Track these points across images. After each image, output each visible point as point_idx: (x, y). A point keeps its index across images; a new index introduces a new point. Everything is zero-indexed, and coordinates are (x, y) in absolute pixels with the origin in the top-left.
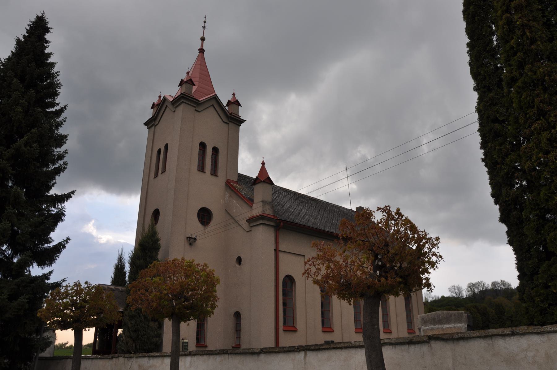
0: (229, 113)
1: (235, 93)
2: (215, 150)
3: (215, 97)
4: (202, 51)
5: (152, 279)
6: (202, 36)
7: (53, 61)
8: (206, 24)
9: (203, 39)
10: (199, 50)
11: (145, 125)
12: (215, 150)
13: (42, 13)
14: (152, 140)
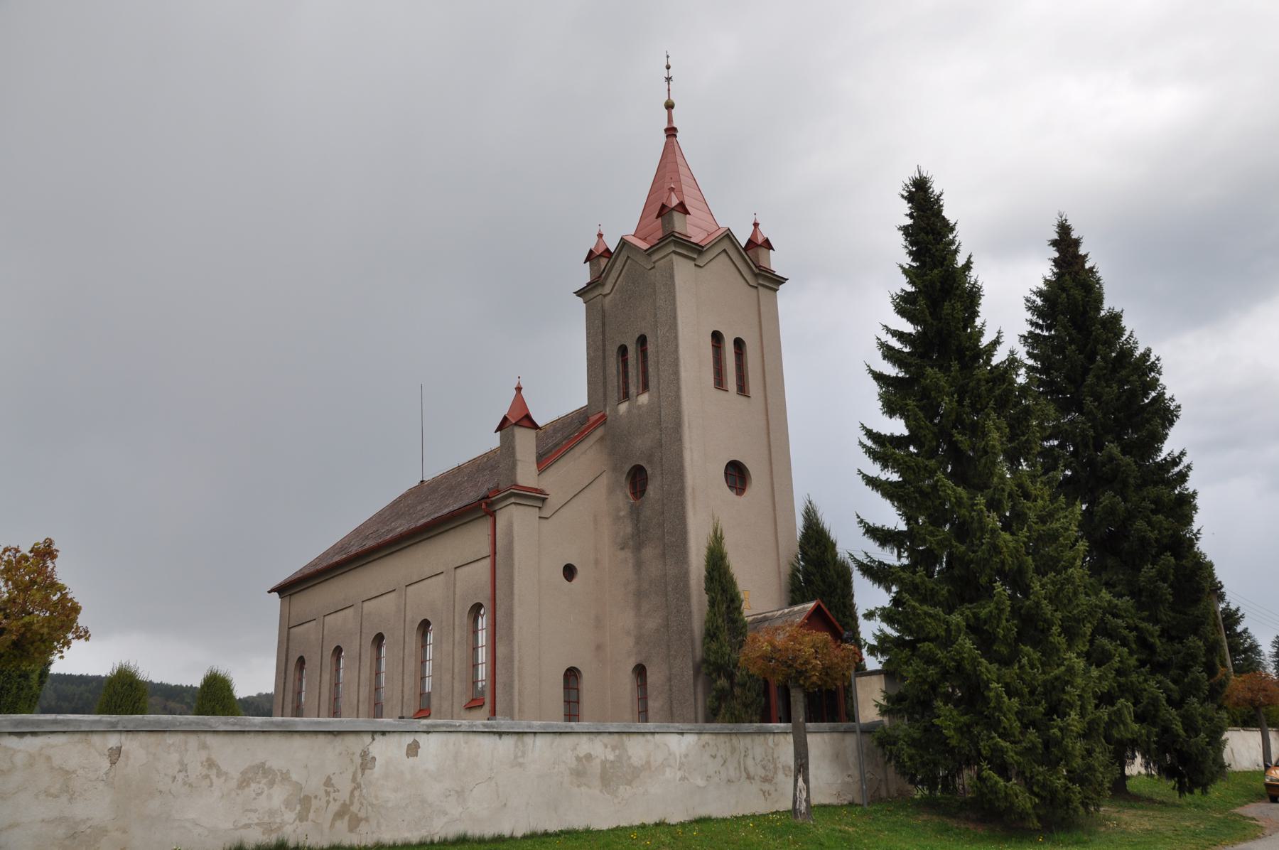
0: (608, 262)
1: (759, 222)
2: (739, 344)
3: (728, 235)
4: (671, 132)
5: (1115, 497)
6: (667, 99)
7: (908, 218)
8: (665, 73)
9: (669, 106)
10: (666, 130)
12: (739, 344)
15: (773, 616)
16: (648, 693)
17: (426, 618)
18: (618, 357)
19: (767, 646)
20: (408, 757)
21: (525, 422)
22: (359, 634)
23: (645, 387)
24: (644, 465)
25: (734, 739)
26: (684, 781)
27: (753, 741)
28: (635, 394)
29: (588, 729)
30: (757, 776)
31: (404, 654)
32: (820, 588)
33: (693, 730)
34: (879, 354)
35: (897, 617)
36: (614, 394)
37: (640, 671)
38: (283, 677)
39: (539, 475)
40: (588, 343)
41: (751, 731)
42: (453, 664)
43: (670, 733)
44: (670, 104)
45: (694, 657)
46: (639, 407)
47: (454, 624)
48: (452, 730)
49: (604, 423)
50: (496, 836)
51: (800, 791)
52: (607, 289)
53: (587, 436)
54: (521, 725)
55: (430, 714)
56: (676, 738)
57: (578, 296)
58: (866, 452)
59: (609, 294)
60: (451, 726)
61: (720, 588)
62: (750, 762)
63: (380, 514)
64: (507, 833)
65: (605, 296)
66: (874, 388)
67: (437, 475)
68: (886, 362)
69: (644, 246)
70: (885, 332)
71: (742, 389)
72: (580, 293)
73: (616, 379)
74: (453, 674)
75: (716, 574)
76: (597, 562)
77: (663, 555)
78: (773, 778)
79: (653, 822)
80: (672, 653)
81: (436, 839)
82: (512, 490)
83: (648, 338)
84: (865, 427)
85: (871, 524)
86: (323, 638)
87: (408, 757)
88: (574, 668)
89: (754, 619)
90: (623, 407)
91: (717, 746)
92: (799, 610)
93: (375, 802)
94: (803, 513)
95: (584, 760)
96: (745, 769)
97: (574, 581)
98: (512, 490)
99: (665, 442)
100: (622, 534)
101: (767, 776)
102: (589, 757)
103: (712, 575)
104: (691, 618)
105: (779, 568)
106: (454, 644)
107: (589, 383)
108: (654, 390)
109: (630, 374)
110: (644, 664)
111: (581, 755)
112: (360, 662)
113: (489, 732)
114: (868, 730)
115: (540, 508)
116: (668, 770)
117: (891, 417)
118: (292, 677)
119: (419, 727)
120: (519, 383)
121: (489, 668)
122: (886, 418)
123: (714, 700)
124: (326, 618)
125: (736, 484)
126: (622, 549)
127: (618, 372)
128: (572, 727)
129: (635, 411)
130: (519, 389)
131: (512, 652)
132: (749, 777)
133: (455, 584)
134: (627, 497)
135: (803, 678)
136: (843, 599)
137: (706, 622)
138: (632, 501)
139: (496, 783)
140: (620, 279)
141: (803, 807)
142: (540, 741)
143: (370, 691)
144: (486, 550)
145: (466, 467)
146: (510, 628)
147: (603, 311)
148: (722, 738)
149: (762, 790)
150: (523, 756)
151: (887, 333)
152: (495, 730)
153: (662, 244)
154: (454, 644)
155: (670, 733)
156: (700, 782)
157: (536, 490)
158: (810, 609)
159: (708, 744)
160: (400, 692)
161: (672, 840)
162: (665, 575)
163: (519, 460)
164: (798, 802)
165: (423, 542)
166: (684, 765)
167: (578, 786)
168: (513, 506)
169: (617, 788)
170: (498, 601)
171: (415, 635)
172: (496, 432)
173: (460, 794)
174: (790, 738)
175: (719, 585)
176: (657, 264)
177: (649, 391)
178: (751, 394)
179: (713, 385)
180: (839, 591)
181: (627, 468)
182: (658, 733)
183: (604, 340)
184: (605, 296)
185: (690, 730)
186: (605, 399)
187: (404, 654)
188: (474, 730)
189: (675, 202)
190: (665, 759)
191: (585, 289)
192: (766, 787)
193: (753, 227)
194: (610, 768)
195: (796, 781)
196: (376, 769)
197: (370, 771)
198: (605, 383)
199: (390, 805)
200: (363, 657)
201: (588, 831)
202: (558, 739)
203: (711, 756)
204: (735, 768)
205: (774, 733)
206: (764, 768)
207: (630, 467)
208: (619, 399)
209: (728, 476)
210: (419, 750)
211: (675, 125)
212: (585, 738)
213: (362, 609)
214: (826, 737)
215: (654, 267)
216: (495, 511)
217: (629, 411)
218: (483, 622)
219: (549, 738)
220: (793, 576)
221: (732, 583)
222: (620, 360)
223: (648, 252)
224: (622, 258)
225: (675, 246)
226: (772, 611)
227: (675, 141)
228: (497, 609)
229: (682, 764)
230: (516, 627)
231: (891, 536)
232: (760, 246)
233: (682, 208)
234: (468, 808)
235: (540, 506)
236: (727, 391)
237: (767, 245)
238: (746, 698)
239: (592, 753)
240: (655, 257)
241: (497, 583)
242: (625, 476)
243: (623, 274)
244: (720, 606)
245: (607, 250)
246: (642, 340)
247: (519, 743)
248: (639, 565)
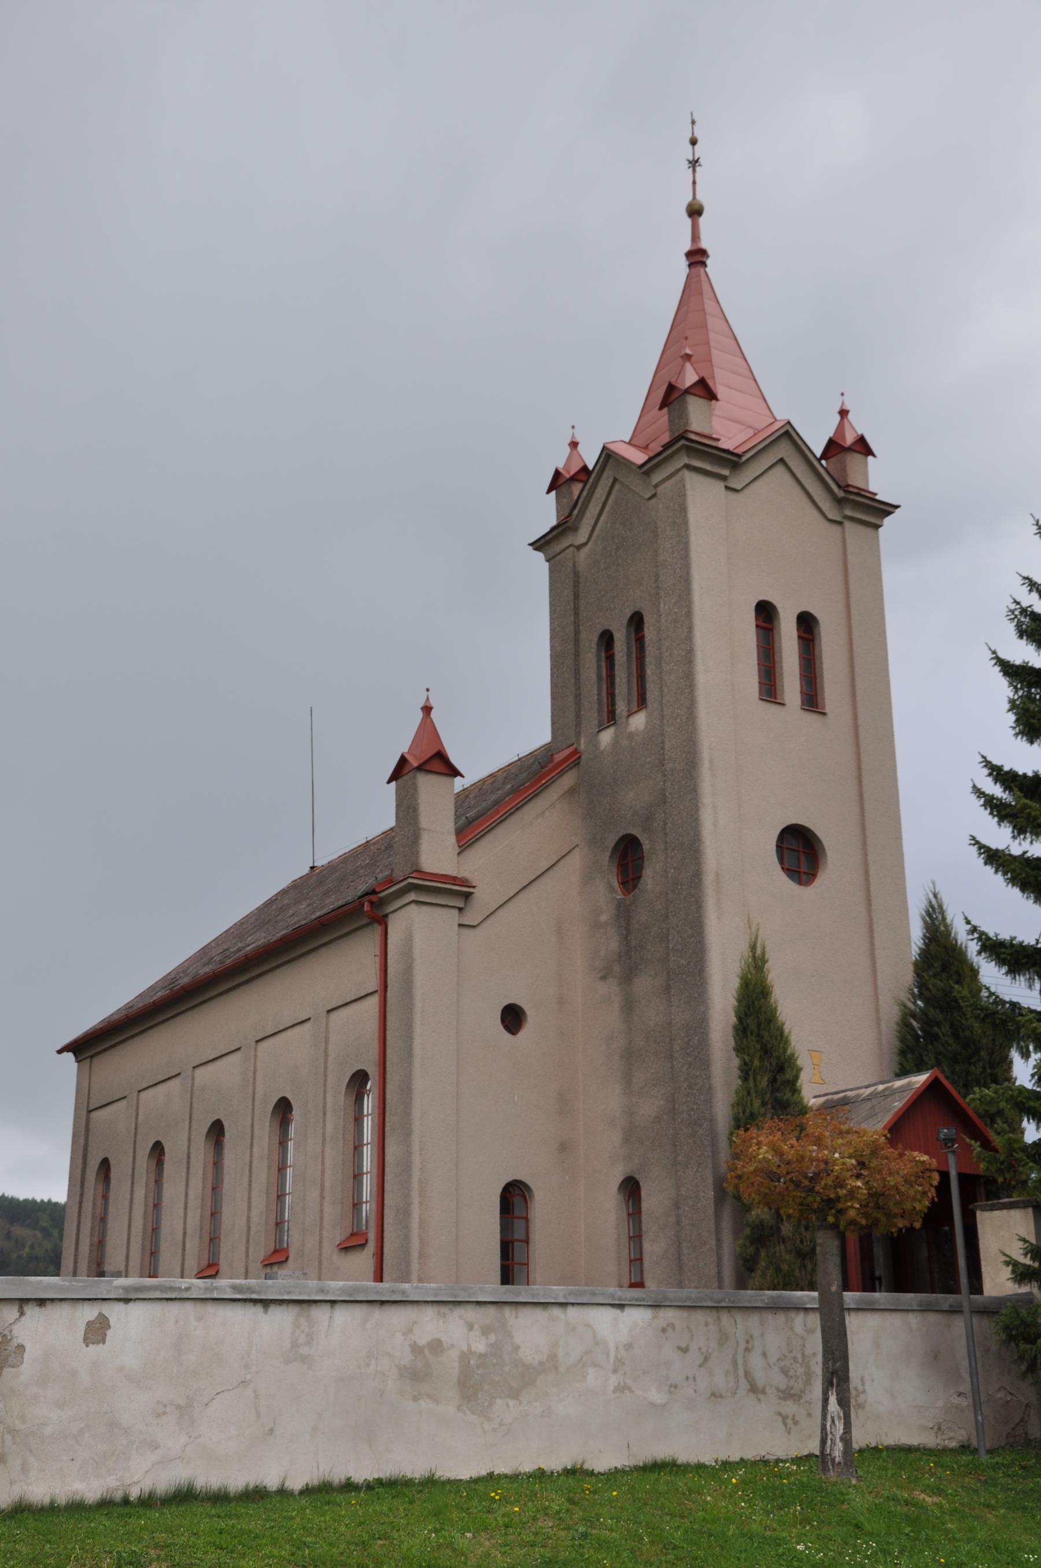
2: (807, 623)
3: (787, 433)
4: (697, 257)
9: (695, 212)
10: (689, 254)
11: (537, 549)
12: (807, 623)
13: (1035, 523)
14: (857, 670)
15: (859, 1096)
16: (644, 1229)
17: (285, 1095)
18: (599, 650)
19: (767, 1152)
20: (87, 1346)
21: (437, 765)
22: (187, 1122)
23: (642, 702)
24: (638, 836)
25: (726, 1319)
26: (623, 1392)
27: (762, 1322)
28: (625, 714)
29: (435, 1296)
30: (771, 1386)
31: (251, 1156)
32: (949, 1048)
33: (643, 1300)
34: (1011, 628)
35: (1032, 1104)
36: (591, 715)
37: (631, 1188)
38: (79, 1193)
39: (459, 854)
40: (552, 630)
41: (760, 1304)
42: (323, 1172)
43: (598, 1304)
44: (696, 207)
45: (715, 1167)
46: (631, 736)
47: (325, 1106)
48: (173, 1296)
49: (577, 764)
50: (251, 1486)
51: (833, 1421)
52: (581, 536)
53: (546, 787)
54: (309, 1289)
55: (287, 1259)
56: (609, 1313)
57: (536, 549)
58: (985, 805)
59: (585, 544)
60: (172, 1289)
61: (758, 1046)
62: (756, 1362)
63: (242, 923)
64: (272, 1483)
65: (579, 548)
66: (1003, 690)
67: (336, 856)
68: (1024, 642)
69: (638, 457)
70: (1026, 589)
71: (812, 700)
72: (540, 545)
73: (595, 687)
74: (322, 1189)
75: (752, 1023)
76: (561, 1001)
77: (667, 989)
78: (803, 1391)
79: (559, 1468)
80: (680, 1158)
81: (134, 1494)
82: (410, 880)
83: (645, 617)
84: (990, 762)
85: (992, 935)
86: (136, 1128)
87: (87, 1346)
88: (515, 1181)
89: (827, 1100)
90: (606, 737)
91: (691, 1331)
92: (902, 1086)
93: (19, 1426)
94: (923, 913)
95: (427, 1352)
96: (747, 1374)
97: (522, 1034)
98: (410, 880)
99: (670, 794)
100: (602, 953)
101: (792, 1388)
102: (436, 1346)
103: (745, 1024)
104: (710, 1099)
105: (877, 1010)
106: (324, 1140)
107: (553, 698)
108: (655, 706)
109: (617, 680)
110: (637, 1176)
111: (422, 1342)
112: (188, 1168)
113: (245, 1300)
114: (990, 1310)
115: (460, 909)
116: (592, 1373)
117: (1032, 743)
118: (92, 1192)
119: (109, 1291)
120: (428, 699)
121: (375, 1180)
122: (1022, 743)
123: (747, 1244)
124: (143, 1095)
125: (799, 866)
126: (604, 978)
127: (599, 677)
128: (403, 1292)
129: (625, 743)
130: (427, 709)
131: (409, 1153)
132: (754, 1389)
133: (327, 1038)
134: (612, 889)
135: (834, 1211)
136: (991, 1067)
137: (733, 1106)
138: (620, 896)
139: (255, 1391)
140: (602, 518)
141: (837, 1452)
142: (342, 1316)
143: (202, 1217)
144: (372, 983)
145: (375, 844)
146: (407, 1113)
147: (576, 574)
148: (700, 1317)
149: (780, 1414)
150: (308, 1344)
151: (1031, 591)
152: (254, 1296)
153: (670, 451)
154: (324, 1140)
155: (598, 1304)
156: (656, 1396)
157: (454, 880)
158: (918, 1086)
159: (672, 1326)
160: (245, 1219)
161: (567, 1505)
162: (670, 1024)
163: (425, 830)
164: (829, 1442)
165: (282, 969)
166: (623, 1364)
167: (415, 1399)
168: (413, 906)
169: (490, 1405)
170: (389, 1068)
171: (268, 1124)
172: (389, 782)
173: (185, 1411)
174: (814, 1320)
175: (758, 1042)
176: (659, 489)
177: (646, 707)
178: (827, 710)
179: (757, 695)
180: (983, 1053)
181: (612, 840)
182: (573, 1304)
183: (576, 624)
184: (579, 548)
185: (637, 1300)
186: (578, 725)
187: (251, 1156)
188: (215, 1296)
189: (690, 377)
190: (586, 1353)
191: (547, 538)
192: (790, 1408)
193: (838, 418)
194: (478, 1367)
195: (826, 1401)
196: (25, 1367)
197: (13, 1370)
198: (578, 697)
199: (48, 1431)
200: (193, 1160)
201: (430, 1482)
202: (378, 1315)
203: (679, 1348)
204: (727, 1373)
205: (806, 1310)
206: (785, 1372)
207: (617, 838)
208: (600, 724)
209: (786, 852)
210: (109, 1333)
211: (704, 244)
212: (430, 1312)
213: (193, 1079)
214: (913, 1319)
215: (654, 495)
216: (386, 916)
217: (616, 742)
218: (369, 1104)
219: (359, 1311)
220: (904, 1024)
221: (781, 1037)
222: (603, 655)
223: (644, 469)
224: (605, 483)
225: (688, 456)
226: (858, 1088)
227: (703, 277)
228: (388, 1080)
229: (619, 1362)
230: (416, 1112)
231: (1027, 956)
232: (849, 449)
233: (705, 390)
234: (199, 1436)
235: (462, 905)
236: (824, 714)
237: (863, 447)
238: (802, 1241)
239: (443, 1339)
240: (656, 478)
241: (388, 1037)
242: (608, 854)
243: (607, 509)
244: (759, 1078)
245: (585, 468)
246: (637, 621)
247: (303, 1320)
248: (629, 1006)
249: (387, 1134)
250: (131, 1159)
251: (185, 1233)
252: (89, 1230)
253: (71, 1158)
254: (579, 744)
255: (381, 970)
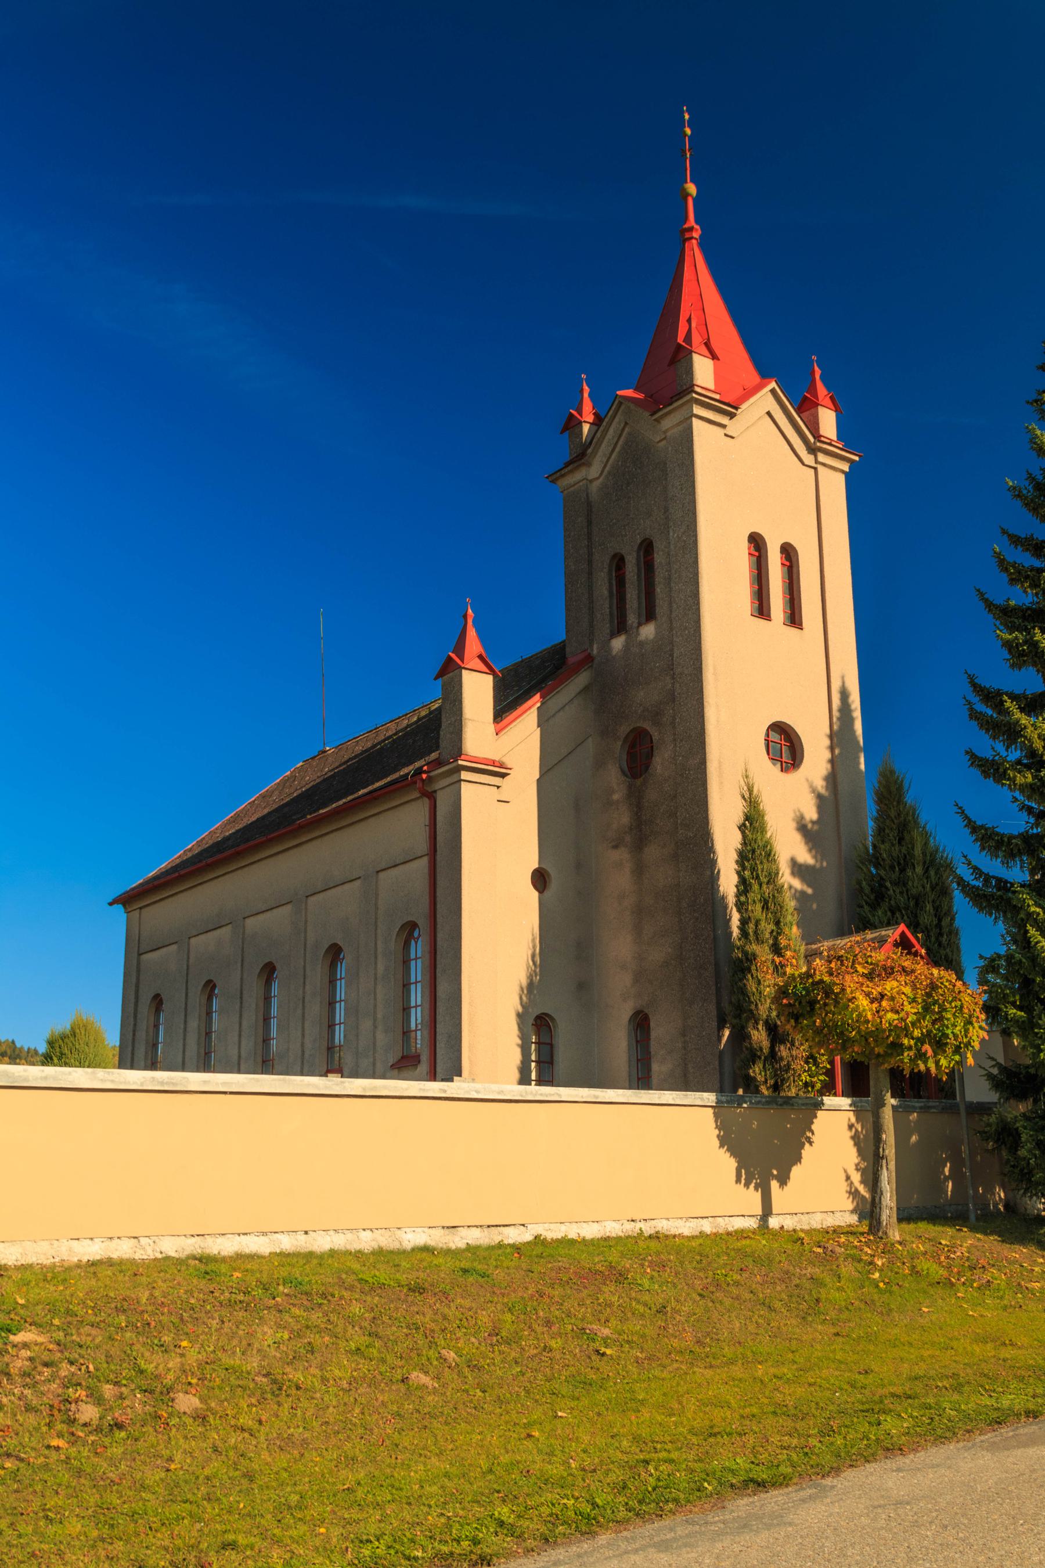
22: (239, 964)
23: (650, 615)
24: (648, 728)
28: (635, 625)
31: (304, 992)
46: (642, 644)
59: (598, 478)
71: (794, 619)
73: (607, 602)
74: (375, 1020)
86: (188, 969)
90: (618, 643)
106: (376, 979)
109: (628, 596)
128: (560, 1095)
154: (376, 979)
187: (304, 992)
207: (628, 730)
213: (244, 927)
216: (435, 791)
217: (627, 647)
243: (617, 449)
246: (647, 548)
249: (438, 975)
250: (184, 995)
251: (239, 1057)
252: (144, 1053)
253: (123, 994)
254: (592, 650)
255: (430, 837)
